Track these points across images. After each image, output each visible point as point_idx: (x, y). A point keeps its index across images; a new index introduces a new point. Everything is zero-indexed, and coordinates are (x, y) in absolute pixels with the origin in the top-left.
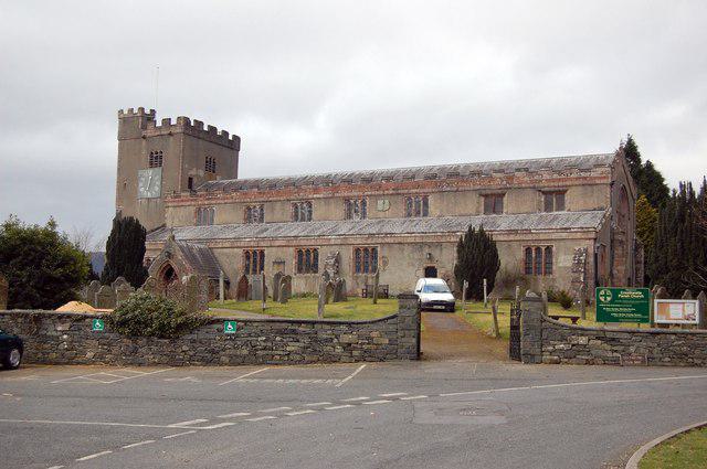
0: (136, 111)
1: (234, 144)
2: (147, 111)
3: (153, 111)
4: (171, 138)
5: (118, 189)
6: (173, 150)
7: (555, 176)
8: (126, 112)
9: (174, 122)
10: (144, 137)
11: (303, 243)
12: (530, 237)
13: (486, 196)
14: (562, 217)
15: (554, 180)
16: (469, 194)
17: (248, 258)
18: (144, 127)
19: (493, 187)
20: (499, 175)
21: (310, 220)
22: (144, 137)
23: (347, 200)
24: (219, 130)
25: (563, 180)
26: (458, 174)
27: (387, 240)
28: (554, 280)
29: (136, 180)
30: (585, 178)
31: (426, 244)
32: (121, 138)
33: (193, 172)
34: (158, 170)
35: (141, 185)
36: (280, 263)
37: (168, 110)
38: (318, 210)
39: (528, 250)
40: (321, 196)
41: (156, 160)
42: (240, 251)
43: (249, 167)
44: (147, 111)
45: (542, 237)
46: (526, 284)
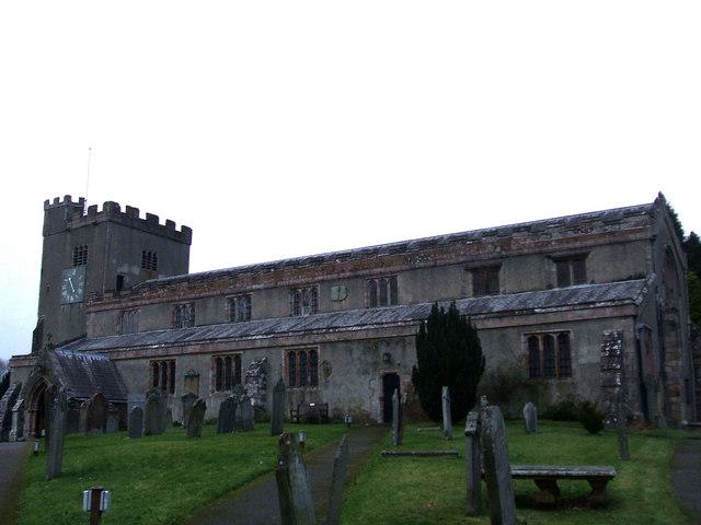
0: (61, 200)
2: (75, 200)
7: (571, 234)
15: (568, 240)
21: (249, 318)
22: (69, 230)
23: (293, 289)
24: (162, 222)
25: (576, 239)
30: (612, 233)
34: (82, 268)
36: (193, 377)
41: (80, 258)
42: (146, 363)
44: (75, 200)
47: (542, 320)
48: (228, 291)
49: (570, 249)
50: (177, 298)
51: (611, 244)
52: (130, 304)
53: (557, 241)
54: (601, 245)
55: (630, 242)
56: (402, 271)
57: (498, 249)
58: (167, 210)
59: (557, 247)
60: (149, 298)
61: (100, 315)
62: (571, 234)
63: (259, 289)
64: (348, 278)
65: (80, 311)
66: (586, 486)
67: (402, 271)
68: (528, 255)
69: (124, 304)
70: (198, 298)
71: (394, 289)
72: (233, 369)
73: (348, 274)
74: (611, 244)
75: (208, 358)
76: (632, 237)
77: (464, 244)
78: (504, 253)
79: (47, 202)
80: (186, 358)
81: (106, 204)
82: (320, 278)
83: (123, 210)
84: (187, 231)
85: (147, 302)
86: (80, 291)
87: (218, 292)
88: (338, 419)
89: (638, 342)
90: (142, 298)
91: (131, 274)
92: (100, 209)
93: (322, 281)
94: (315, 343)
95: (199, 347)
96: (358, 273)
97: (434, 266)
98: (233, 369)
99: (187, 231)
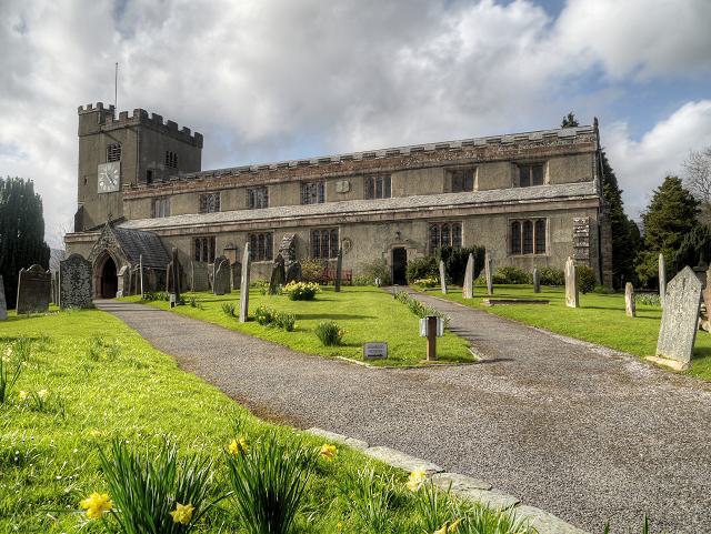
0: (94, 106)
1: (197, 141)
2: (106, 107)
3: (112, 108)
5: (80, 185)
6: (130, 142)
8: (85, 108)
9: (131, 115)
10: (103, 132)
11: (255, 226)
12: (517, 209)
13: (454, 172)
14: (547, 190)
16: (500, 164)
17: (198, 245)
18: (103, 122)
20: (469, 148)
21: (266, 206)
22: (103, 132)
23: (303, 183)
24: (180, 129)
26: (249, 171)
29: (95, 175)
31: (393, 222)
32: (82, 135)
33: (152, 166)
35: (100, 179)
37: (125, 102)
39: (515, 225)
40: (277, 180)
41: (114, 154)
43: (210, 162)
45: (533, 208)
47: (525, 209)
48: (249, 183)
51: (565, 155)
52: (163, 193)
54: (557, 156)
55: (580, 153)
56: (396, 171)
57: (475, 156)
58: (74, 122)
64: (351, 176)
65: (116, 198)
66: (342, 288)
67: (396, 171)
71: (388, 184)
74: (565, 155)
76: (582, 150)
79: (81, 108)
81: (136, 111)
83: (150, 117)
84: (199, 137)
89: (599, 227)
91: (157, 170)
92: (131, 115)
93: (329, 178)
99: (199, 137)
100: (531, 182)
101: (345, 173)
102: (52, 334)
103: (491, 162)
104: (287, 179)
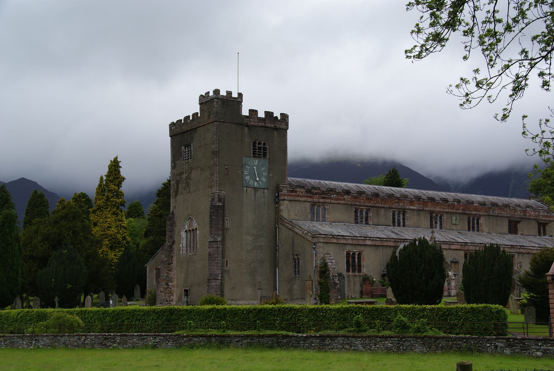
0: (211, 94)
4: (276, 133)
7: (546, 214)
19: (516, 216)
23: (431, 213)
25: (547, 216)
27: (522, 250)
28: (290, 361)
38: (411, 219)
40: (415, 208)
46: (328, 346)
48: (394, 206)
49: (545, 220)
50: (358, 203)
53: (542, 215)
57: (522, 214)
59: (542, 218)
60: (337, 199)
61: (294, 203)
62: (546, 214)
63: (413, 210)
64: (460, 214)
68: (532, 219)
69: (315, 200)
70: (373, 207)
72: (356, 261)
73: (461, 211)
75: (462, 253)
77: (509, 208)
78: (524, 216)
80: (450, 251)
82: (447, 210)
85: (336, 202)
86: (264, 179)
87: (388, 206)
88: (208, 336)
90: (332, 199)
94: (515, 253)
95: (459, 246)
96: (465, 212)
97: (497, 216)
98: (356, 261)
100: (315, 219)
101: (458, 211)
102: (316, 262)
103: (529, 219)
104: (422, 208)
